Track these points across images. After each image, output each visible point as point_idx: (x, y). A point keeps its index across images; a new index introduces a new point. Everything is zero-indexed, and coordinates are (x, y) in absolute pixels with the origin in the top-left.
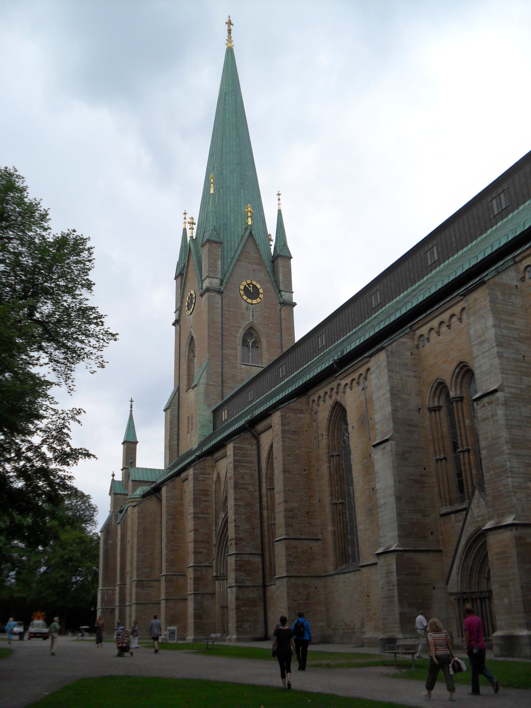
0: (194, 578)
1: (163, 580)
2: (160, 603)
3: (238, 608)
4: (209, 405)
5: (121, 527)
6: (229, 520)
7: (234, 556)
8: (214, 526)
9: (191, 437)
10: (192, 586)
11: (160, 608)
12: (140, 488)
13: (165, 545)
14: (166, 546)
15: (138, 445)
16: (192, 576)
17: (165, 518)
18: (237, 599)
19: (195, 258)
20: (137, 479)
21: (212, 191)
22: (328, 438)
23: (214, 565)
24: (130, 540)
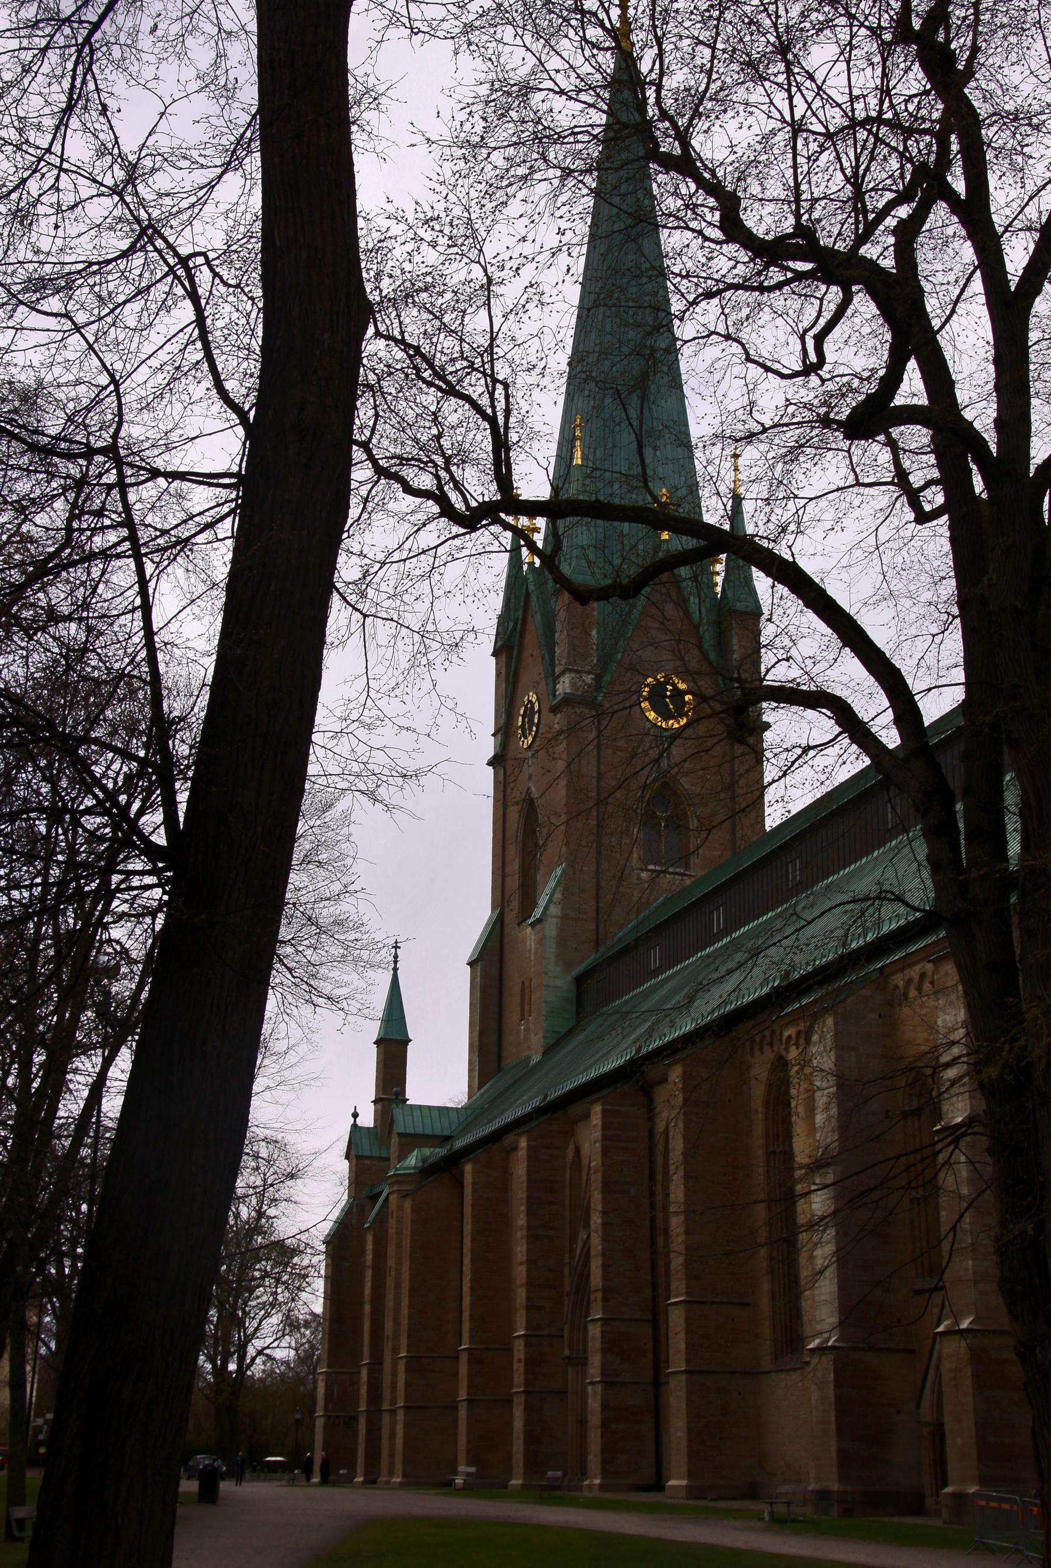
0: (526, 1359)
1: (464, 1359)
2: (457, 1408)
3: (605, 1424)
4: (568, 966)
5: (375, 1237)
6: (593, 1253)
7: (599, 1323)
8: (567, 1255)
9: (527, 1029)
10: (522, 1377)
11: (456, 1420)
12: (415, 1153)
13: (469, 1285)
14: (472, 1288)
15: (410, 1047)
16: (522, 1356)
17: (470, 1227)
18: (604, 1407)
19: (538, 618)
20: (410, 1130)
21: (578, 460)
22: (766, 1119)
23: (566, 1333)
24: (393, 1266)
